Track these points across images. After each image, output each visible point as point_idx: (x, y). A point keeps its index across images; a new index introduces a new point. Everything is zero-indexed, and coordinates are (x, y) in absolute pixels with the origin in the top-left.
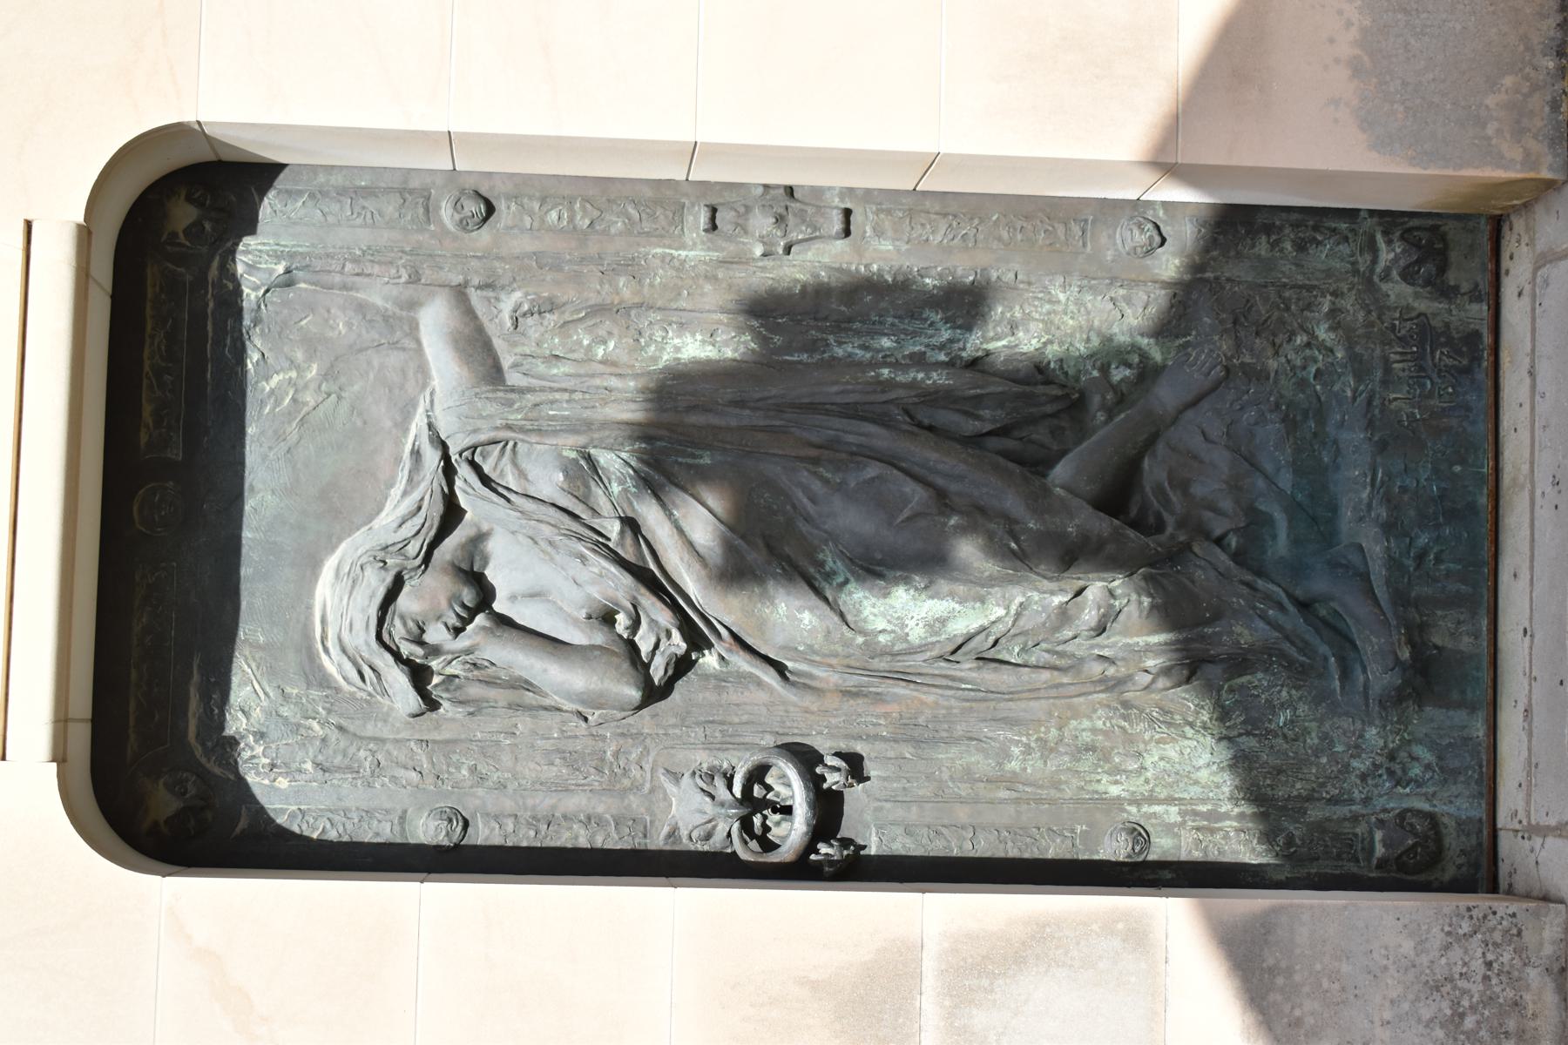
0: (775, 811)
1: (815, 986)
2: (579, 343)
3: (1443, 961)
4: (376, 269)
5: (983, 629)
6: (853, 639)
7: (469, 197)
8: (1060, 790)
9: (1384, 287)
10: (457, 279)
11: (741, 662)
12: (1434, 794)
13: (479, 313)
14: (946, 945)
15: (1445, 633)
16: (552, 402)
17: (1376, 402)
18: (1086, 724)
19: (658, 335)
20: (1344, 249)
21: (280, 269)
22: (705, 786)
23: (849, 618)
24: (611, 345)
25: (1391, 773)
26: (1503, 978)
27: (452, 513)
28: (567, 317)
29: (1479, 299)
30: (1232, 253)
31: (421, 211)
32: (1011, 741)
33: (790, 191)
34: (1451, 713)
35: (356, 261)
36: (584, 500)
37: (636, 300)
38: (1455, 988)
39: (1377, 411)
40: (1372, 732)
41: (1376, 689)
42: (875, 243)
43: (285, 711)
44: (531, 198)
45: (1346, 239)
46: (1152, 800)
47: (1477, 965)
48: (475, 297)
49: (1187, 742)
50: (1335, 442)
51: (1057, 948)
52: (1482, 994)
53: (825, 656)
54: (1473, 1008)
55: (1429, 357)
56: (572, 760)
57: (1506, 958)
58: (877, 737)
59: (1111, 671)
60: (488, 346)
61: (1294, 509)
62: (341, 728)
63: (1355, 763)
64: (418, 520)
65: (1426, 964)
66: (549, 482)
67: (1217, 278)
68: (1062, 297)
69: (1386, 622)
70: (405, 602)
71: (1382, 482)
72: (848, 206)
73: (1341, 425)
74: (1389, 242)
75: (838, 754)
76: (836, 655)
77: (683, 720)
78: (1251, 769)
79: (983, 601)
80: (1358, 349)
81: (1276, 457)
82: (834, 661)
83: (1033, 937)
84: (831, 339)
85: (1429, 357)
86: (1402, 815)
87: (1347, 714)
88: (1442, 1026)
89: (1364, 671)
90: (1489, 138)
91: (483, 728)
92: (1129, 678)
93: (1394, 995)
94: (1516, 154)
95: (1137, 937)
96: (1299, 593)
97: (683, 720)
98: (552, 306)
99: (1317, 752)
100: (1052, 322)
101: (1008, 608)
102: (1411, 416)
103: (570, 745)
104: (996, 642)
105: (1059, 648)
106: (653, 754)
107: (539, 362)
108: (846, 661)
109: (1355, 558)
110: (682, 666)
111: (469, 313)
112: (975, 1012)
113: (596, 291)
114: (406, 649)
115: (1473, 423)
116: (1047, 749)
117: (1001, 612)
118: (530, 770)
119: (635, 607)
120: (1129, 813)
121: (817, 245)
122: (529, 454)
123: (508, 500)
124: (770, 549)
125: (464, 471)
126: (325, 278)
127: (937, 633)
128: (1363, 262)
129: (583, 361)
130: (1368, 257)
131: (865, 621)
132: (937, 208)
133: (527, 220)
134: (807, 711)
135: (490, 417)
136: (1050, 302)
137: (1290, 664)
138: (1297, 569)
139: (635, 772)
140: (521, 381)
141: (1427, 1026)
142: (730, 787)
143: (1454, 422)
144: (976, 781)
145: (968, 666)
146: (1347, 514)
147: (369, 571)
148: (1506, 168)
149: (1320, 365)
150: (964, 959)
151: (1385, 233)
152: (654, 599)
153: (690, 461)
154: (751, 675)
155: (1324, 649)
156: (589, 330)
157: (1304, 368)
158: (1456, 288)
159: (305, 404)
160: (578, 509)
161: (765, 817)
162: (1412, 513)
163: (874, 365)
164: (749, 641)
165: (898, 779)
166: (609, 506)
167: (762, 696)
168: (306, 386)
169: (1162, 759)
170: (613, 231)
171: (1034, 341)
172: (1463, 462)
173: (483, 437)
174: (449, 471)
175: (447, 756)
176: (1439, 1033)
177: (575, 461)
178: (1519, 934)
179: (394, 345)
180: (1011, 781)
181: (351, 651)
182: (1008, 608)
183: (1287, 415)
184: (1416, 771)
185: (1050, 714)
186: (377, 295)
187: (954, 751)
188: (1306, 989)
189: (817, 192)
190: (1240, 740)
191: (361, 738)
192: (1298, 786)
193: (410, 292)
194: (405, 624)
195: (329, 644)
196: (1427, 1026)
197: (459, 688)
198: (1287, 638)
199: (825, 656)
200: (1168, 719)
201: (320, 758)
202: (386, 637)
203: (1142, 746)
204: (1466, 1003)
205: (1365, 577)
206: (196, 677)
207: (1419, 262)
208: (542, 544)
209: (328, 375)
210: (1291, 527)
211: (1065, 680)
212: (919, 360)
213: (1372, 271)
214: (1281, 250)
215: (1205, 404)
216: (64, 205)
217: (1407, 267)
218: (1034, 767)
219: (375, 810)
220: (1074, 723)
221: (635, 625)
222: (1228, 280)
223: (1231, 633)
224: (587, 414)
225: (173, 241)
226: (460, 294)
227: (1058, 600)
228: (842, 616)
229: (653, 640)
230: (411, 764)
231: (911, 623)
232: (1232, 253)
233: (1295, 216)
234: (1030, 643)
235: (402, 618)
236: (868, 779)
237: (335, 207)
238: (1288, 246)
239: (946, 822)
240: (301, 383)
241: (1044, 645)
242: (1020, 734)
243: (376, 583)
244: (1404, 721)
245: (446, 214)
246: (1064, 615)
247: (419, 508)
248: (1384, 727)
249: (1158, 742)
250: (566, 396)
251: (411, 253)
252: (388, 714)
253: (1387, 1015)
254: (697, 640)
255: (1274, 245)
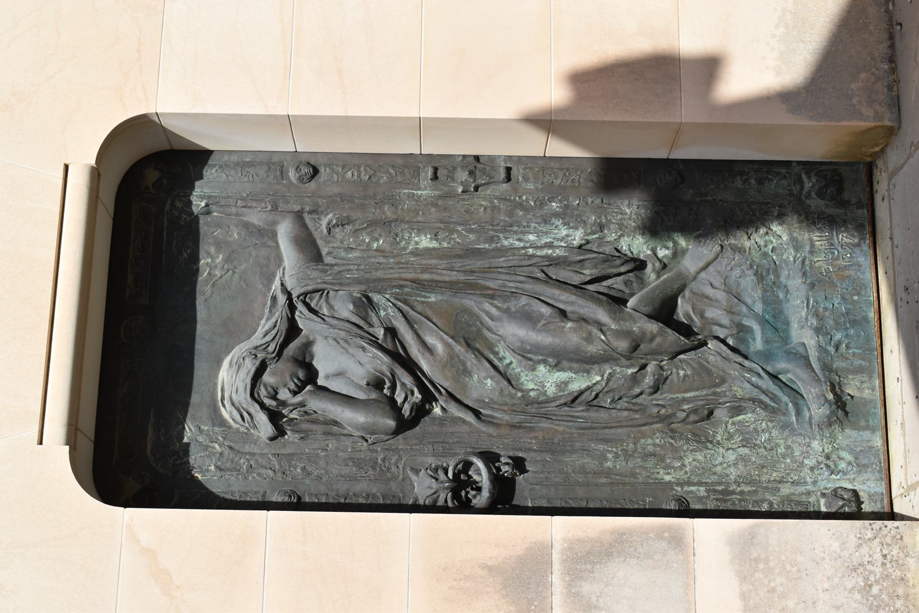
0: (472, 489)
1: (490, 569)
2: (364, 241)
3: (857, 554)
4: (254, 204)
5: (588, 388)
6: (516, 394)
7: (304, 165)
8: (636, 478)
9: (808, 202)
10: (297, 208)
11: (455, 411)
12: (854, 479)
13: (310, 227)
14: (566, 545)
15: (852, 387)
16: (348, 270)
17: (807, 263)
18: (650, 441)
19: (407, 236)
20: (785, 182)
21: (203, 204)
22: (432, 474)
23: (513, 382)
24: (381, 242)
25: (828, 466)
26: (894, 564)
27: (293, 330)
28: (357, 227)
29: (862, 207)
30: (722, 186)
31: (278, 173)
32: (607, 451)
33: (477, 158)
34: (861, 433)
35: (243, 199)
36: (365, 319)
37: (394, 217)
38: (865, 570)
39: (808, 268)
40: (816, 444)
41: (816, 419)
42: (524, 185)
43: (200, 439)
44: (337, 166)
45: (785, 177)
46: (689, 483)
47: (878, 557)
48: (307, 218)
49: (708, 451)
50: (786, 286)
51: (630, 547)
52: (882, 573)
53: (500, 405)
54: (877, 582)
55: (835, 238)
56: (359, 463)
57: (895, 552)
58: (531, 450)
59: (663, 411)
60: (314, 243)
61: (763, 322)
62: (231, 448)
63: (806, 462)
64: (274, 332)
65: (847, 556)
66: (345, 310)
67: (714, 200)
68: (628, 211)
69: (819, 380)
70: (267, 378)
71: (813, 306)
72: (509, 165)
73: (789, 277)
74: (809, 178)
75: (510, 457)
76: (506, 405)
77: (421, 441)
78: (746, 466)
79: (588, 372)
80: (795, 235)
81: (753, 295)
82: (506, 408)
83: (616, 541)
84: (501, 235)
85: (835, 238)
86: (835, 490)
87: (800, 434)
88: (859, 592)
89: (809, 410)
90: (854, 105)
91: (308, 448)
92: (674, 414)
93: (829, 574)
94: (870, 113)
95: (677, 541)
96: (769, 369)
97: (421, 441)
98: (348, 221)
99: (784, 456)
100: (623, 224)
101: (602, 376)
102: (828, 271)
103: (357, 456)
104: (597, 396)
105: (634, 401)
106: (404, 460)
107: (342, 251)
108: (513, 408)
109: (801, 350)
110: (421, 411)
111: (304, 226)
112: (583, 584)
113: (373, 213)
114: (268, 402)
115: (863, 273)
116: (628, 456)
117: (599, 378)
118: (335, 470)
119: (393, 376)
120: (676, 491)
121: (492, 187)
122: (335, 297)
123: (324, 320)
124: (468, 345)
125: (300, 307)
126: (228, 210)
127: (563, 391)
128: (796, 189)
129: (365, 250)
130: (798, 187)
131: (522, 384)
132: (557, 166)
133: (335, 177)
134: (490, 435)
135: (315, 278)
136: (621, 213)
137: (765, 407)
138: (767, 356)
139: (394, 469)
140: (333, 261)
141: (850, 592)
142: (446, 473)
143: (852, 273)
144: (587, 473)
145: (581, 409)
146: (794, 325)
147: (247, 360)
148: (865, 121)
149: (775, 245)
150: (576, 554)
151: (806, 174)
152: (402, 370)
153: (423, 299)
154: (460, 418)
155: (785, 399)
156: (369, 234)
157: (766, 246)
158: (849, 202)
159: (215, 276)
160: (362, 323)
161: (467, 493)
162: (831, 322)
163: (524, 248)
164: (458, 396)
165: (543, 472)
166: (378, 322)
167: (466, 428)
168: (216, 267)
169: (694, 460)
170: (381, 182)
171: (613, 235)
172: (859, 294)
173: (310, 288)
174: (292, 307)
175: (289, 462)
176: (858, 596)
177: (360, 299)
178: (901, 538)
179: (264, 245)
180: (608, 473)
181: (237, 405)
182: (602, 376)
183: (757, 271)
184: (842, 465)
185: (629, 436)
186: (255, 217)
187: (574, 457)
188: (777, 571)
189: (492, 158)
190: (739, 450)
191: (242, 453)
192: (774, 475)
193: (270, 218)
194: (266, 389)
195: (225, 402)
196: (850, 592)
197: (296, 424)
198: (764, 392)
199: (500, 405)
200: (697, 438)
201: (219, 463)
202: (256, 395)
203: (682, 454)
204: (872, 578)
205: (806, 359)
206: (152, 420)
207: (826, 186)
208: (342, 342)
209: (227, 260)
210: (763, 333)
211: (637, 416)
212: (550, 246)
213: (801, 194)
214: (749, 184)
215: (711, 268)
216: (85, 155)
217: (820, 189)
218: (621, 465)
219: (248, 492)
220: (643, 441)
221: (393, 388)
222: (720, 200)
223: (731, 390)
224: (367, 276)
225: (149, 196)
226: (299, 217)
227: (630, 371)
228: (509, 381)
229: (403, 396)
230: (269, 466)
231: (548, 385)
232: (722, 186)
233: (756, 166)
234: (617, 397)
235: (265, 386)
236: (528, 471)
237: (233, 172)
238: (753, 182)
239: (571, 496)
240: (213, 265)
241: (625, 399)
242: (612, 447)
243: (250, 366)
244: (833, 438)
245: (292, 175)
246: (635, 379)
247: (275, 326)
248: (822, 440)
249: (692, 451)
250: (356, 267)
251: (273, 195)
252: (257, 440)
253: (826, 586)
254: (428, 397)
255: (745, 181)
